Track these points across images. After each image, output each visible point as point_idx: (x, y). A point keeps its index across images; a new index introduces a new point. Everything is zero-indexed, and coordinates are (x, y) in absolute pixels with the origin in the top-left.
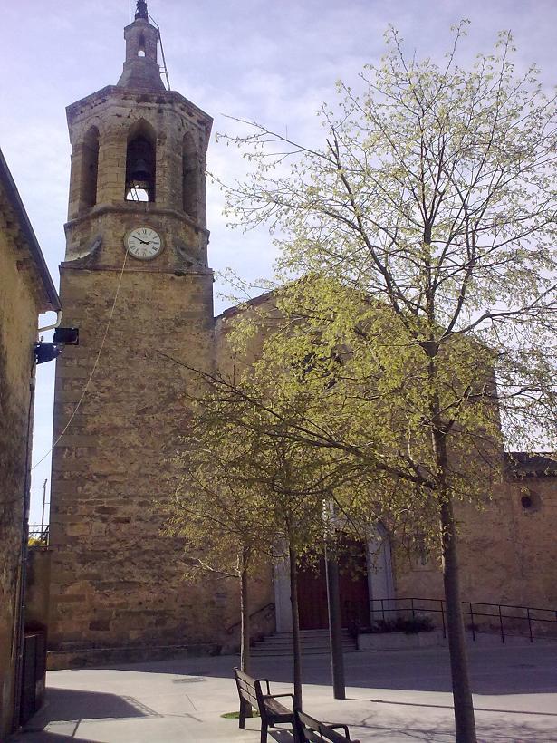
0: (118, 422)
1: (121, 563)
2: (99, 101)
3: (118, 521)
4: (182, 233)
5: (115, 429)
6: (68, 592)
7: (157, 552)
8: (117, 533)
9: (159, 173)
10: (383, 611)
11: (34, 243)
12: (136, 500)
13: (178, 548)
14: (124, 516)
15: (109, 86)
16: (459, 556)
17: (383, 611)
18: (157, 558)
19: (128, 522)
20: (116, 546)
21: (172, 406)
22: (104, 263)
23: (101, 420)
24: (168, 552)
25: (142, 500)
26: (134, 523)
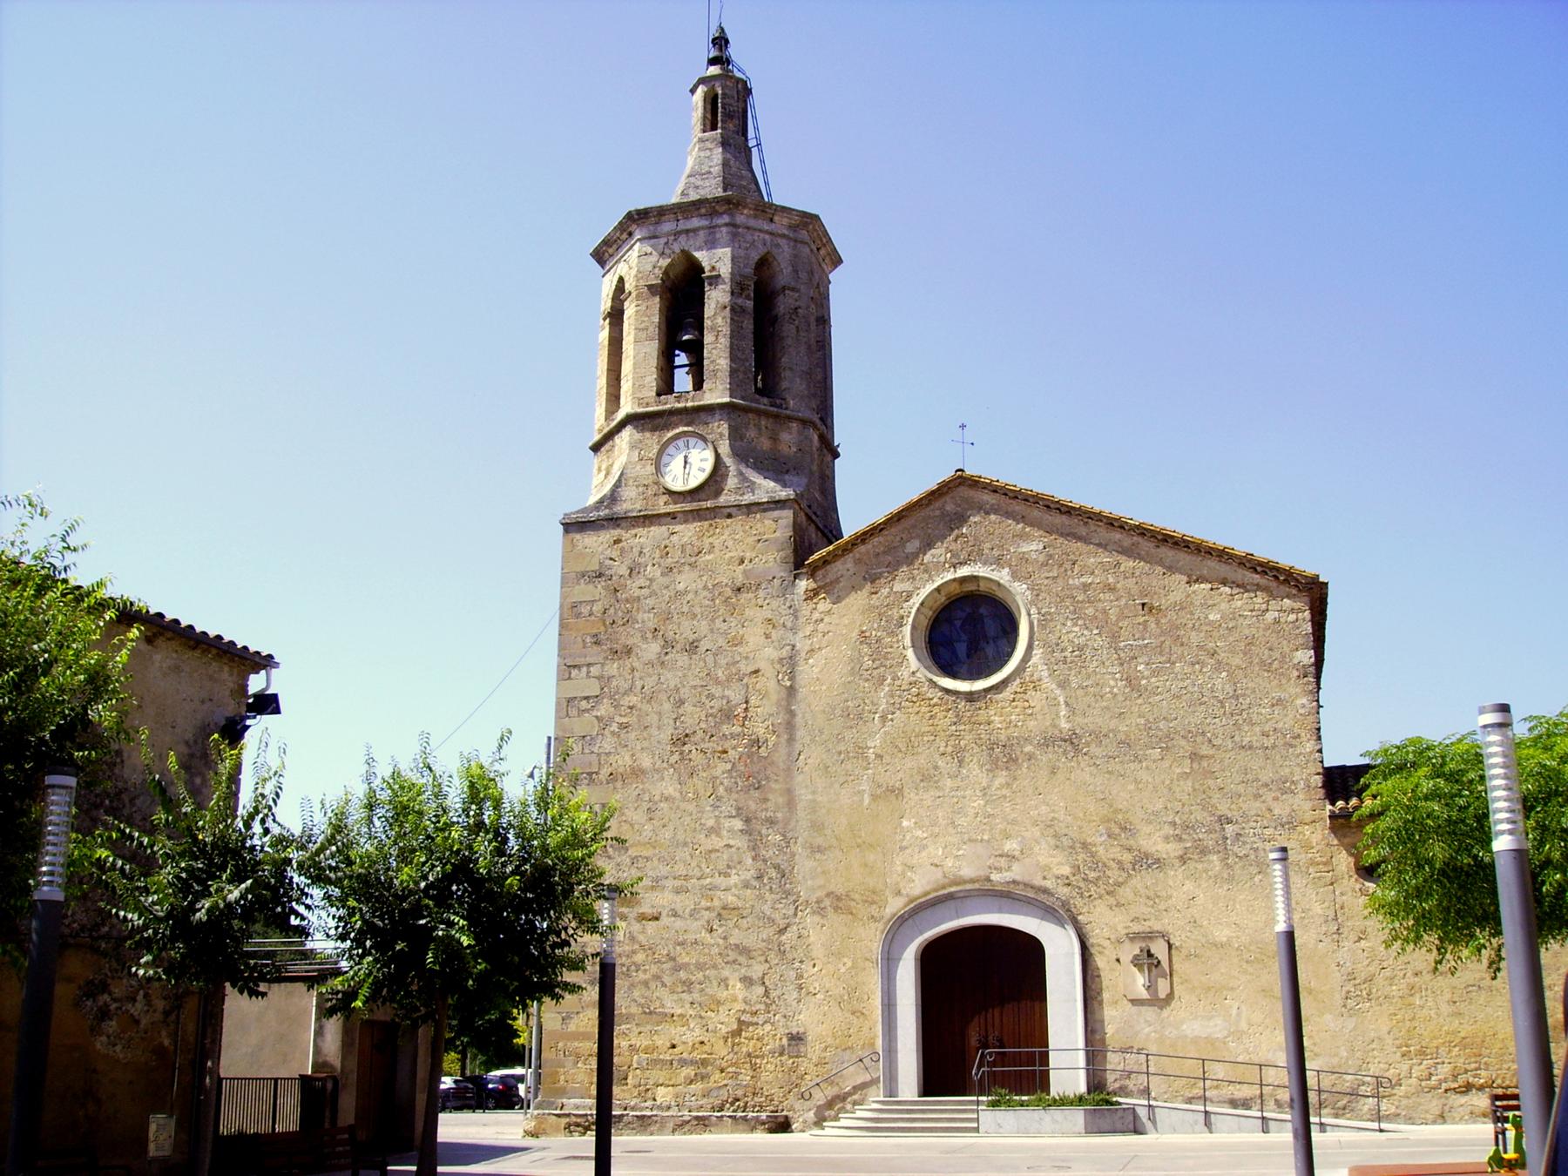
0: (646, 762)
1: (646, 984)
2: (624, 236)
3: (642, 918)
4: (751, 433)
5: (637, 773)
6: (572, 1027)
7: (700, 967)
8: (641, 938)
9: (708, 338)
10: (1204, 1080)
11: (829, 402)
12: (669, 883)
13: (730, 959)
14: (650, 911)
15: (630, 212)
16: (1101, 961)
17: (1148, 1073)
18: (700, 975)
19: (657, 919)
20: (640, 957)
21: (727, 730)
22: (624, 506)
23: (623, 761)
24: (715, 967)
25: (678, 883)
26: (665, 920)
